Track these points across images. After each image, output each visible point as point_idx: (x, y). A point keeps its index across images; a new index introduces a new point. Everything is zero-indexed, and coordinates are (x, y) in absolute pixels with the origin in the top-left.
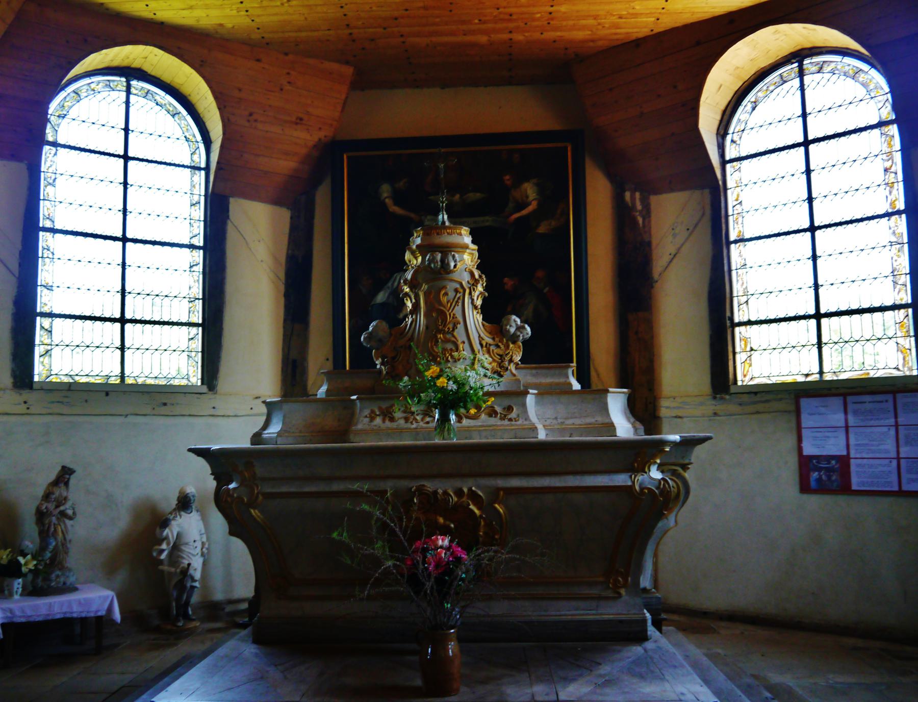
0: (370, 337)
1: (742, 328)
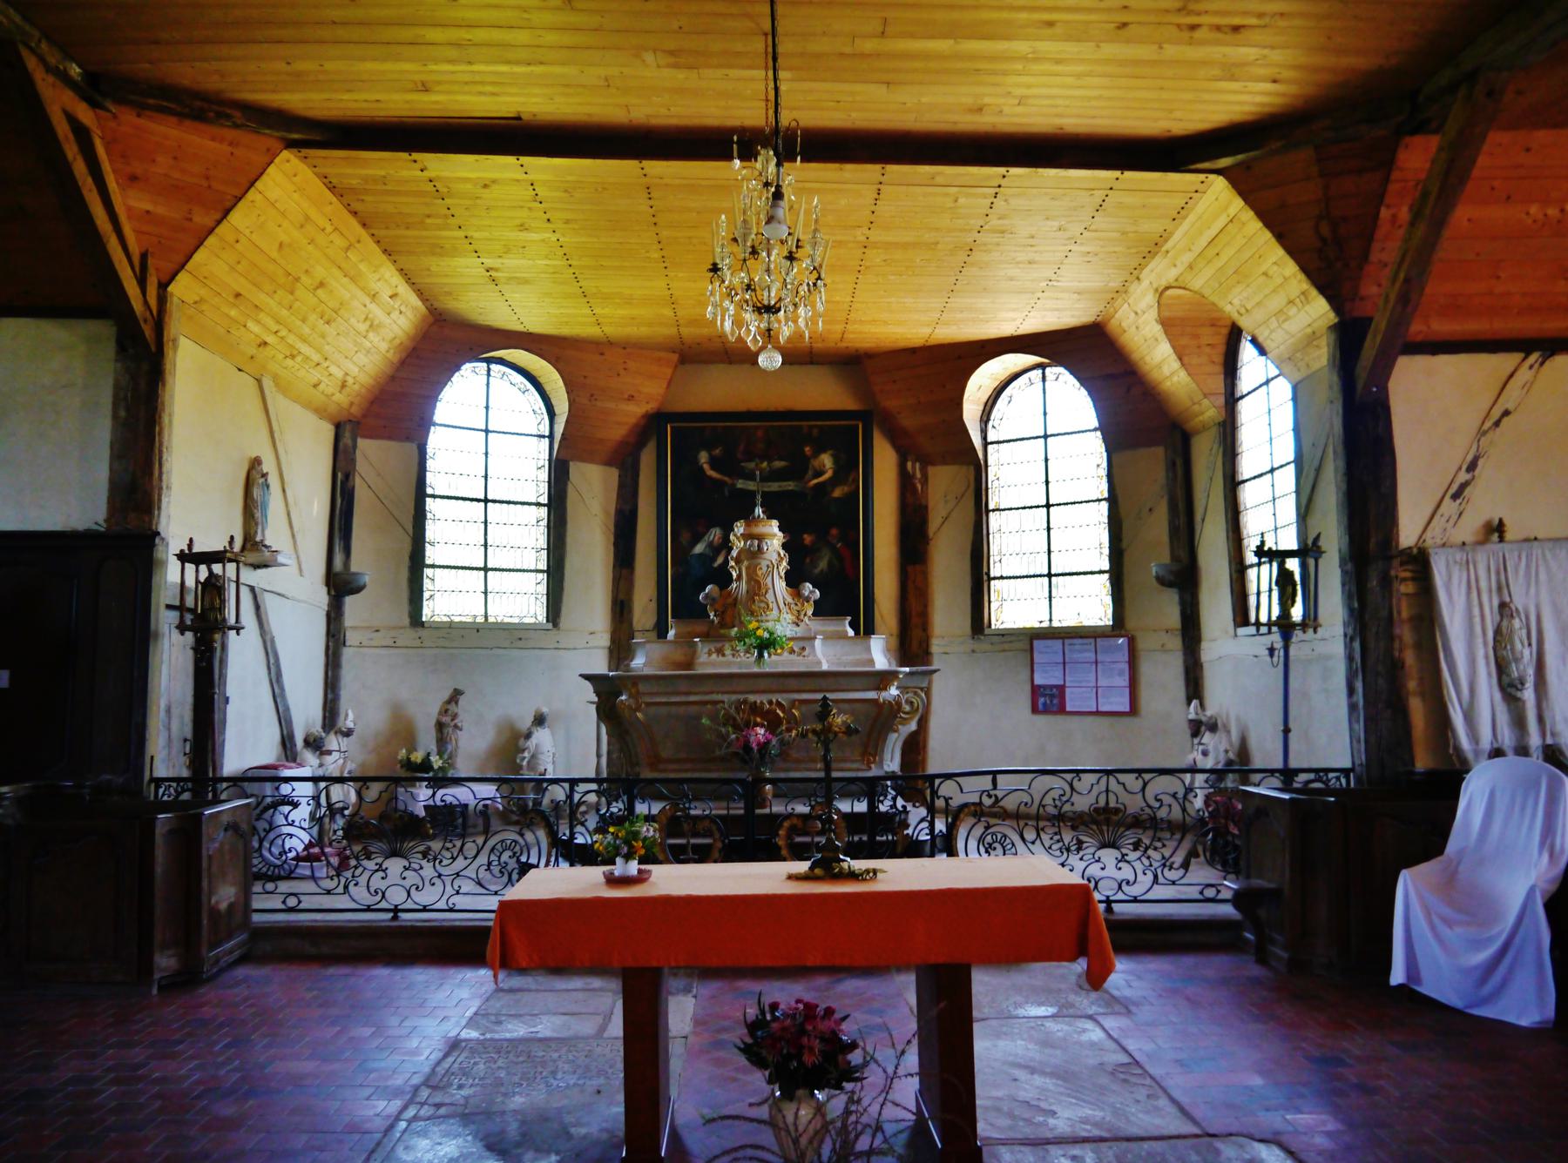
0: (707, 596)
1: (997, 581)
